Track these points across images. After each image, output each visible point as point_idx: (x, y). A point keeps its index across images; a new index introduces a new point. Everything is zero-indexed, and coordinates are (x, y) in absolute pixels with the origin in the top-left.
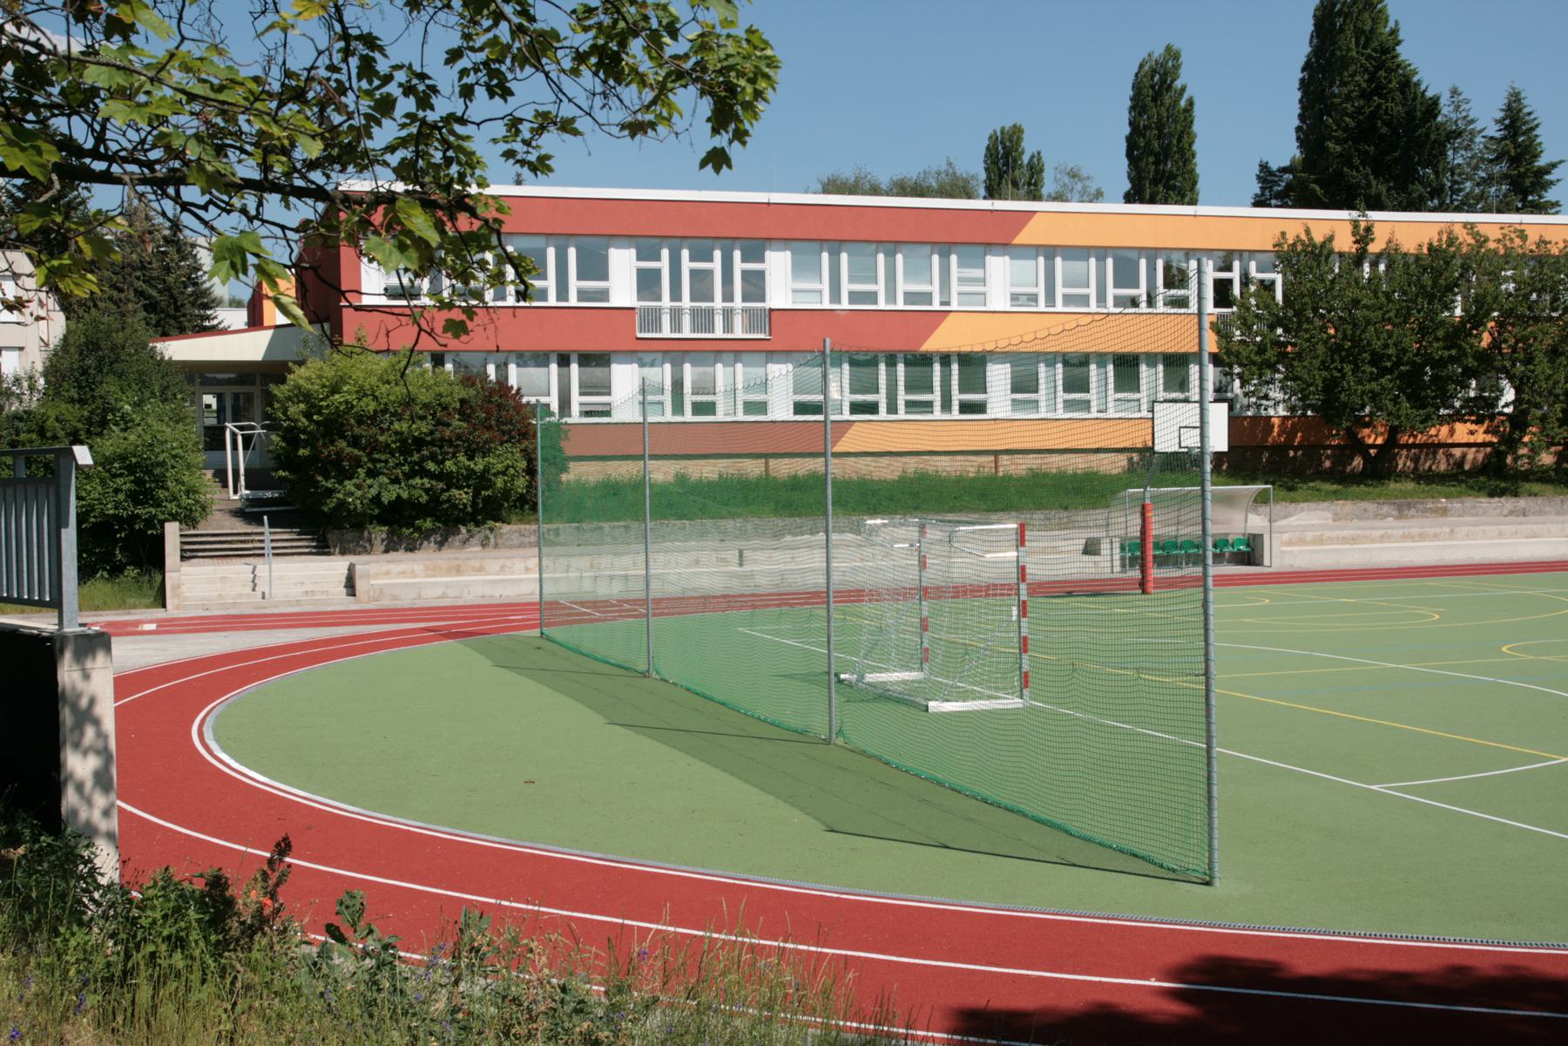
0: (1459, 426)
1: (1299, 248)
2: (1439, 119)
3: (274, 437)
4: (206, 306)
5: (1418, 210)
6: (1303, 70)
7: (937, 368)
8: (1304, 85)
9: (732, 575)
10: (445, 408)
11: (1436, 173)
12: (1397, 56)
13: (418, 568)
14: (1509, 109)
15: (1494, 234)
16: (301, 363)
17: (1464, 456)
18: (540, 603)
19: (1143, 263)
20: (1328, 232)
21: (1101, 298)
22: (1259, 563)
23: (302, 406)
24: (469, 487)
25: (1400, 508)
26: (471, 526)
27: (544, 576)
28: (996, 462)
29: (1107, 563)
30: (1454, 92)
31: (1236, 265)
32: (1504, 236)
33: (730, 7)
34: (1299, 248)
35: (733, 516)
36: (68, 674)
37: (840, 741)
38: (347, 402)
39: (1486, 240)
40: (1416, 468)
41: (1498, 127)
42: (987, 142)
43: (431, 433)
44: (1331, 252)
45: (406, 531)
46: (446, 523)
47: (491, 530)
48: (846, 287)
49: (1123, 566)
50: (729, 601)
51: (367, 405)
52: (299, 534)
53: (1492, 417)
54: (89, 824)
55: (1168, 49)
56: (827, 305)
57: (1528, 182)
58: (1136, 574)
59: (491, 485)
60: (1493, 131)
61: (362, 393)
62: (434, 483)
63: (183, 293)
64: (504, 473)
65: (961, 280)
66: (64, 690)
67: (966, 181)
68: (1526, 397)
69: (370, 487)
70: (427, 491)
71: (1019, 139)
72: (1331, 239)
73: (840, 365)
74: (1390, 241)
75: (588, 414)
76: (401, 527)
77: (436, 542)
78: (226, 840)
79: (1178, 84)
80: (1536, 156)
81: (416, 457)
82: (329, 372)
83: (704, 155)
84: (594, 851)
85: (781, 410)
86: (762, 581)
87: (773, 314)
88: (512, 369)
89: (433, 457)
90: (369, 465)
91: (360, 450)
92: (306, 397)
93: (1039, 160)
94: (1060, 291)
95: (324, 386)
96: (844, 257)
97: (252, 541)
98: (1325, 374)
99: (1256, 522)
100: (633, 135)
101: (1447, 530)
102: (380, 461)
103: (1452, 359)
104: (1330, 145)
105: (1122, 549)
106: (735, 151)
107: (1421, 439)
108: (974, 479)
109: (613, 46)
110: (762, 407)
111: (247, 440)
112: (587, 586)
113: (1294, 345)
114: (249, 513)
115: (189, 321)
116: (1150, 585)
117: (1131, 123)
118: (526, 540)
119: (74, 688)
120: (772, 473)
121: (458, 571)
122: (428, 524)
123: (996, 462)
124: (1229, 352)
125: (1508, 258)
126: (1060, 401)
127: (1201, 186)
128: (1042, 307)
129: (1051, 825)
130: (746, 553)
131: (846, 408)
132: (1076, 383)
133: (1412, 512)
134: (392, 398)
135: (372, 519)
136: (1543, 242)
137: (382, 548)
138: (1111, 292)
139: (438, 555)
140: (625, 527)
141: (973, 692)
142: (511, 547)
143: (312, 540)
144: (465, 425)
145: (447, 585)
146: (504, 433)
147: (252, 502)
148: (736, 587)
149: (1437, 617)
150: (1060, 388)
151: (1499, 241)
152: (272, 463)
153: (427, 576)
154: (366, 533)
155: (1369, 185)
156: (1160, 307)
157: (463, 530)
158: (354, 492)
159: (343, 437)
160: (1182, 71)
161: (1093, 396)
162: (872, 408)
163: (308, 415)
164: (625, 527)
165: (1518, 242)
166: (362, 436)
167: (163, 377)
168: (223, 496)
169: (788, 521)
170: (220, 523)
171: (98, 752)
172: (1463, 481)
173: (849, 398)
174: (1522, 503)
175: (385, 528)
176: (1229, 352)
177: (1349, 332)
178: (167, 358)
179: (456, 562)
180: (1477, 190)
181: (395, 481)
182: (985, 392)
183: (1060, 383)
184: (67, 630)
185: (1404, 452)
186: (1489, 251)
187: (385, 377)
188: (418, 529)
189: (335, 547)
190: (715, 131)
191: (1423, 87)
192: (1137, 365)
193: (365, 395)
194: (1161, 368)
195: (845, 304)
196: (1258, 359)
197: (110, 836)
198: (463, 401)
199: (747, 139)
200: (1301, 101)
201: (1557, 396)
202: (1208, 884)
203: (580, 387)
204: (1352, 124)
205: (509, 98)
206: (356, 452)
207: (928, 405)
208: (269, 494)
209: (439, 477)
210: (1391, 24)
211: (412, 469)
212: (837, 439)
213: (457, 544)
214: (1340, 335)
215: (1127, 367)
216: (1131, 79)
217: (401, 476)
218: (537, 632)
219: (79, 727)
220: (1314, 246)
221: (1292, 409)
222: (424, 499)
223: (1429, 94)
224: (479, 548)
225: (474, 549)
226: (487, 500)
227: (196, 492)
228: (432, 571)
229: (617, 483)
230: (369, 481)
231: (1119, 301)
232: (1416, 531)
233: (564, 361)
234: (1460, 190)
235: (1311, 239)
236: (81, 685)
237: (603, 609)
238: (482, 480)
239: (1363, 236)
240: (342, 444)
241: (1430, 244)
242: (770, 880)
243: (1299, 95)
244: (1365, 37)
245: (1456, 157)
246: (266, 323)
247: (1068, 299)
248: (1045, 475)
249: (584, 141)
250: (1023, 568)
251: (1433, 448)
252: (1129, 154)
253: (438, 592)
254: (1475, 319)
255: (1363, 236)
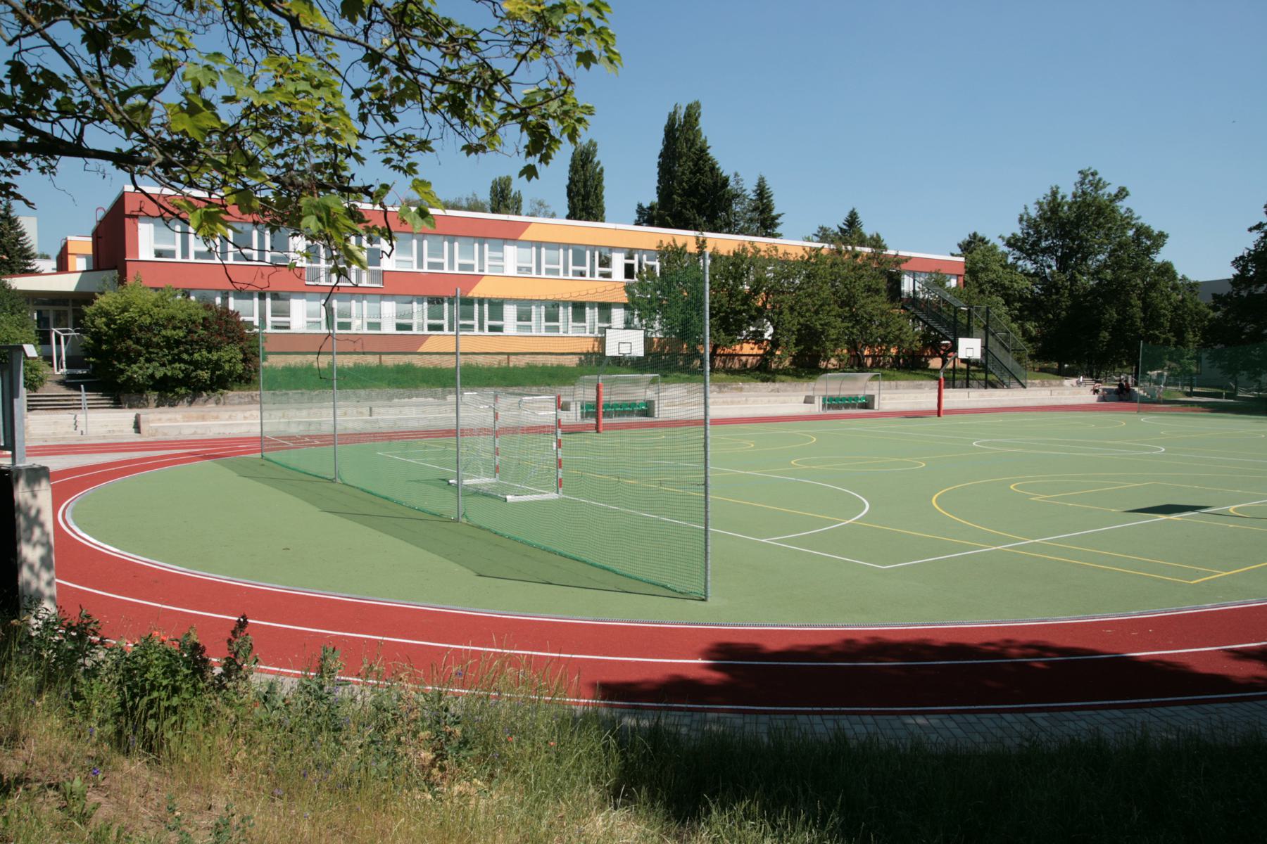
0: (745, 345)
1: (670, 249)
2: (729, 188)
3: (85, 338)
4: (28, 258)
5: (720, 232)
6: (660, 157)
7: (476, 306)
8: (660, 165)
9: (366, 422)
10: (194, 322)
11: (727, 214)
12: (708, 154)
13: (179, 416)
14: (759, 185)
15: (763, 248)
16: (102, 293)
17: (747, 361)
18: (261, 437)
19: (588, 253)
20: (684, 242)
21: (566, 272)
22: (652, 416)
23: (104, 319)
24: (208, 369)
25: (720, 387)
26: (210, 392)
27: (264, 421)
28: (508, 358)
29: (572, 416)
30: (736, 175)
31: (636, 256)
32: (768, 249)
33: (613, 66)
34: (670, 249)
35: (364, 387)
36: (21, 493)
37: (464, 520)
38: (132, 317)
39: (760, 251)
40: (724, 367)
41: (754, 194)
42: (491, 185)
43: (185, 337)
44: (686, 252)
45: (170, 395)
46: (194, 390)
47: (222, 394)
48: (426, 259)
49: (582, 417)
50: (375, 436)
51: (146, 320)
52: (103, 396)
53: (762, 341)
54: (38, 590)
55: (591, 141)
56: (415, 269)
57: (768, 222)
58: (593, 421)
59: (220, 369)
60: (752, 196)
61: (142, 313)
62: (187, 366)
63: (13, 249)
64: (229, 361)
65: (490, 258)
66: (19, 505)
67: (482, 204)
68: (779, 331)
69: (148, 368)
70: (183, 371)
71: (509, 184)
72: (685, 245)
73: (422, 303)
74: (714, 248)
75: (276, 327)
76: (167, 392)
77: (188, 402)
78: (103, 591)
79: (596, 160)
80: (771, 210)
81: (176, 351)
82: (120, 300)
83: (522, 169)
84: (343, 592)
85: (389, 328)
86: (382, 425)
87: (385, 274)
88: (231, 300)
89: (186, 351)
90: (147, 355)
91: (141, 346)
92: (106, 314)
93: (519, 195)
94: (544, 266)
95: (117, 308)
96: (425, 243)
97: (73, 400)
98: (682, 316)
99: (650, 394)
100: (468, 154)
101: (744, 399)
102: (154, 353)
103: (744, 311)
104: (675, 196)
105: (582, 408)
106: (541, 168)
107: (727, 351)
108: (498, 368)
109: (461, 95)
110: (377, 326)
111: (66, 338)
112: (282, 428)
113: (666, 300)
114: (70, 383)
115: (17, 266)
116: (601, 429)
117: (570, 179)
118: (242, 400)
119: (26, 503)
120: (384, 364)
121: (203, 418)
122: (183, 391)
123: (508, 358)
124: (634, 303)
125: (770, 260)
126: (543, 327)
127: (606, 214)
128: (534, 274)
129: (604, 568)
130: (373, 409)
131: (426, 327)
132: (552, 317)
133: (726, 389)
134: (161, 316)
135: (148, 387)
136: (786, 253)
137: (155, 405)
138: (571, 268)
139: (189, 409)
140: (302, 393)
141: (528, 490)
142: (234, 404)
143: (110, 399)
144: (206, 333)
145: (197, 427)
146: (229, 338)
147: (70, 376)
148: (369, 428)
149: (752, 445)
150: (543, 319)
151: (765, 251)
152: (83, 354)
153: (184, 421)
154: (145, 396)
155: (695, 219)
156: (597, 277)
157: (204, 394)
158: (138, 371)
159: (130, 338)
160: (598, 153)
161: (560, 324)
162: (440, 328)
163: (107, 325)
164: (302, 393)
165: (774, 252)
166: (142, 338)
167: (11, 300)
168: (50, 371)
169: (396, 390)
170: (51, 389)
171: (43, 545)
172: (748, 374)
173: (427, 322)
174: (777, 385)
175: (157, 393)
176: (634, 303)
177: (695, 294)
178: (13, 288)
179: (202, 414)
180: (746, 225)
181: (163, 365)
182: (502, 320)
183: (543, 316)
184: (19, 465)
185: (719, 358)
186: (761, 256)
187: (156, 304)
188: (177, 393)
189: (125, 403)
190: (529, 154)
191: (721, 171)
192: (558, 307)
193: (145, 314)
194: (596, 310)
195: (426, 269)
196: (648, 307)
197: (52, 598)
198: (204, 319)
199: (550, 161)
200: (659, 173)
201: (793, 332)
202: (703, 600)
203: (272, 312)
204: (687, 187)
205: (396, 124)
206: (139, 347)
207: (471, 327)
208: (80, 372)
209: (190, 363)
210: (703, 138)
211: (173, 358)
212: (420, 345)
213: (201, 402)
214: (690, 296)
215: (579, 308)
216: (570, 155)
217: (166, 362)
218: (258, 455)
219: (30, 529)
220: (677, 249)
221: (666, 334)
222: (181, 376)
223: (724, 175)
224: (214, 405)
225: (211, 406)
226: (219, 377)
227: (37, 370)
228: (188, 419)
229: (295, 368)
230: (147, 365)
231: (575, 273)
232: (729, 400)
233: (262, 296)
234: (738, 224)
235: (676, 245)
236: (31, 501)
237: (296, 441)
238: (217, 365)
239: (701, 245)
240: (130, 342)
241: (734, 251)
242: (456, 608)
243: (657, 170)
244: (691, 143)
245: (737, 208)
246: (70, 269)
247: (548, 271)
248: (536, 367)
249: (437, 155)
250: (559, 420)
251: (732, 356)
252: (569, 195)
253: (192, 430)
254: (755, 291)
255: (701, 245)
